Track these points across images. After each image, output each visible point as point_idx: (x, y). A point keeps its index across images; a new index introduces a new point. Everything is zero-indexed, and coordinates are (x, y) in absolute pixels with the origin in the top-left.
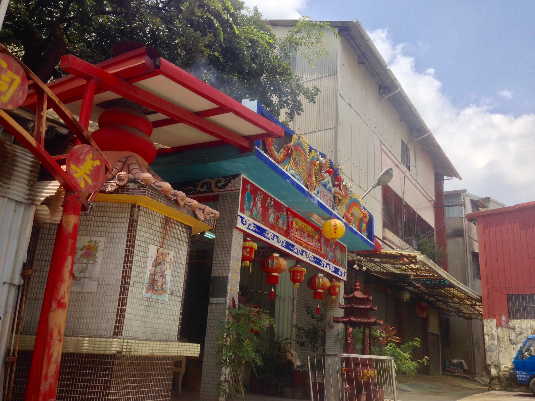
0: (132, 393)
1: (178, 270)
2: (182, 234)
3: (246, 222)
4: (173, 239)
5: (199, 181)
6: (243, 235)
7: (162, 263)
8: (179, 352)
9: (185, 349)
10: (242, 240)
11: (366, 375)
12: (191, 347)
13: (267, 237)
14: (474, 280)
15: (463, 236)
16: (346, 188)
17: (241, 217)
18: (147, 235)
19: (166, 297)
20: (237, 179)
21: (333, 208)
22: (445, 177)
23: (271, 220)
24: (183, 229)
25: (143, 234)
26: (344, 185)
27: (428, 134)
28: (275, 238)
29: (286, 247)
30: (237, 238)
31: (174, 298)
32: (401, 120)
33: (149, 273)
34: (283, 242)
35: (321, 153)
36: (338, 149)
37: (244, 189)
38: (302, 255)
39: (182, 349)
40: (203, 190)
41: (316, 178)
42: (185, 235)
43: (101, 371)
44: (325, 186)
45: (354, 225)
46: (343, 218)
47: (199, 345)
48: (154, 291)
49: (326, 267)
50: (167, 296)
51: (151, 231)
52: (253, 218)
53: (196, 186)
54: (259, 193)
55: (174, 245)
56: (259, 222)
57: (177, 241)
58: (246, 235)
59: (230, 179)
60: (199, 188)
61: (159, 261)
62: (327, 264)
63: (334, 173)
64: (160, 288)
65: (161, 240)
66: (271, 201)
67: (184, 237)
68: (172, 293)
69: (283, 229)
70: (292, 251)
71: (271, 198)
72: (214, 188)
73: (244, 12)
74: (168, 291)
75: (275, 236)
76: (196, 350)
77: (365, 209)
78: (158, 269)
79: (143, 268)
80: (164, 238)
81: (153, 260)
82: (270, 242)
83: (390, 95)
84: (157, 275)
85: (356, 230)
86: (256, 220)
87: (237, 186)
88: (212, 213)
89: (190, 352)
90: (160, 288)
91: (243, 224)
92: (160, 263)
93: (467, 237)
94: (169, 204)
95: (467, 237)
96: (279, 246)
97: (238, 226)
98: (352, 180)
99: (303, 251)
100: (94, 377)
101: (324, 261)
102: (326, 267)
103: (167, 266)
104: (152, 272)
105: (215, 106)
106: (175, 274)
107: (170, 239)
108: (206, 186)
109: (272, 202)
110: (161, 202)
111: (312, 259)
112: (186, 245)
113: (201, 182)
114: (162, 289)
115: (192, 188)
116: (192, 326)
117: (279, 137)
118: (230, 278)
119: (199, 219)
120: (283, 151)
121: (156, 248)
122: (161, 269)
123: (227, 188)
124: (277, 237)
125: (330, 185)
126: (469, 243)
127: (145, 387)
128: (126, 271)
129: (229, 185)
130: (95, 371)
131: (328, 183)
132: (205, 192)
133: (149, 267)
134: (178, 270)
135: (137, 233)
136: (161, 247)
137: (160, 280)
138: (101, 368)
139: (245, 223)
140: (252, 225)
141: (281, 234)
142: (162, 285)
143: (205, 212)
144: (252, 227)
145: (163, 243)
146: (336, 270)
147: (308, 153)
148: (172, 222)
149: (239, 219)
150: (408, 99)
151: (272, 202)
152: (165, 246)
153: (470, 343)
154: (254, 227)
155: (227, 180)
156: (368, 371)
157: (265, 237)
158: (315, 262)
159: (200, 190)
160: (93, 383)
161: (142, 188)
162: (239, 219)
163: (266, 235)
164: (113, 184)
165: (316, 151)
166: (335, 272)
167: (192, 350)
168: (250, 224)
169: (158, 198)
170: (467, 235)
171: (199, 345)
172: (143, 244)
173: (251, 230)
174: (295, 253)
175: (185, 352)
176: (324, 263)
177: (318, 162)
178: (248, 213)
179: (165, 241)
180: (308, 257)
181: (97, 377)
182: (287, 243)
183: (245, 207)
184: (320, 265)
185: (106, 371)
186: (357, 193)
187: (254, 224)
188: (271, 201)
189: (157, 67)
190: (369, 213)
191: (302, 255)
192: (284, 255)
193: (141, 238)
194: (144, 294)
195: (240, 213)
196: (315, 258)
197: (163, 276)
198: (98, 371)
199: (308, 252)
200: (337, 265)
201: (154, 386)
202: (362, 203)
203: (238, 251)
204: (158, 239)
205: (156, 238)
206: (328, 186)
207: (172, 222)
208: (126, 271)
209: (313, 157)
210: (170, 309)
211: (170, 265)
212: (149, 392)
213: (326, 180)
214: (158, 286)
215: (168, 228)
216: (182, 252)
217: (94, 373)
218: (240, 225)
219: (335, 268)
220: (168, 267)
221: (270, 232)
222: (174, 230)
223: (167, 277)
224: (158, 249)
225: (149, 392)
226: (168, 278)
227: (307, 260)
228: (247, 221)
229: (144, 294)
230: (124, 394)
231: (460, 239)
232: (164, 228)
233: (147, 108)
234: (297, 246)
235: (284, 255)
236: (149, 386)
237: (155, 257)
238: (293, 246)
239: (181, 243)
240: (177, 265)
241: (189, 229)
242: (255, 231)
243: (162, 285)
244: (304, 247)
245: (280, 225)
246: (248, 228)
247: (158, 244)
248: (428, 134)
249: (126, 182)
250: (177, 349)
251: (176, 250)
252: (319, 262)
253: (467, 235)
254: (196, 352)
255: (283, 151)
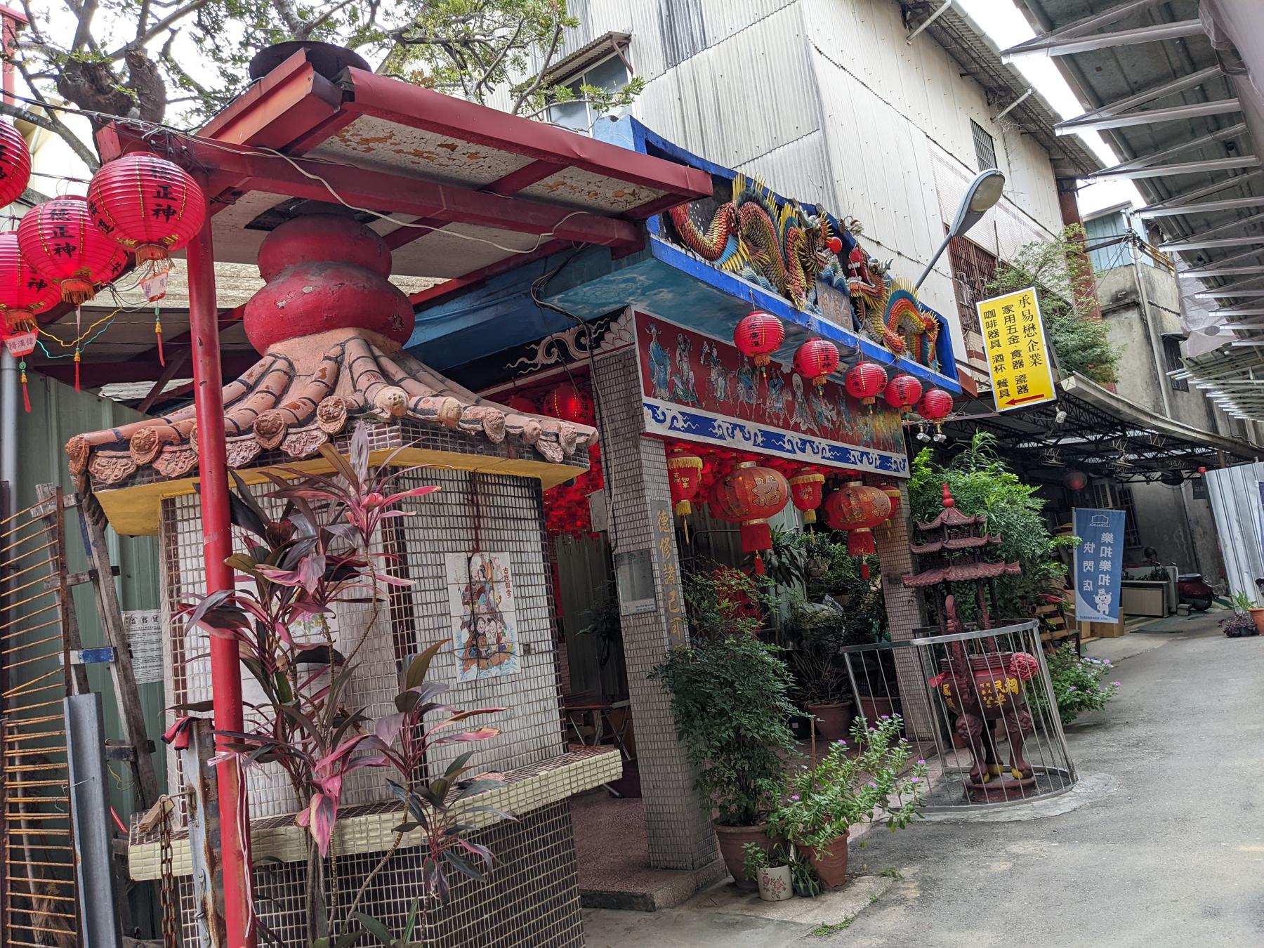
0: (487, 909)
1: (529, 591)
2: (520, 503)
3: (664, 415)
4: (499, 524)
5: (538, 343)
6: (663, 446)
7: (487, 588)
8: (574, 785)
9: (587, 774)
10: (664, 459)
11: (1000, 691)
12: (599, 764)
13: (720, 433)
14: (1175, 395)
15: (1136, 305)
16: (877, 273)
17: (650, 407)
18: (434, 534)
19: (515, 665)
20: (622, 320)
21: (856, 329)
22: (1079, 183)
23: (720, 394)
24: (518, 492)
25: (421, 534)
26: (871, 269)
27: (1030, 91)
28: (737, 432)
29: (766, 444)
30: (651, 457)
31: (534, 659)
32: (961, 75)
33: (460, 623)
34: (756, 435)
35: (805, 206)
36: (836, 178)
37: (644, 339)
38: (803, 450)
39: (581, 776)
40: (552, 360)
41: (805, 268)
42: (527, 503)
43: (400, 882)
44: (829, 281)
45: (908, 353)
46: (882, 344)
47: (618, 751)
48: (483, 662)
49: (861, 461)
50: (518, 661)
51: (441, 522)
52: (679, 401)
53: (533, 354)
54: (680, 339)
55: (506, 535)
56: (693, 406)
57: (511, 524)
58: (670, 445)
59: (608, 323)
60: (541, 359)
61: (478, 587)
62: (863, 454)
63: (845, 245)
64: (494, 648)
65: (471, 534)
66: (711, 349)
67: (523, 506)
68: (527, 650)
69: (750, 405)
70: (781, 448)
71: (710, 341)
72: (573, 351)
73: (1002, 405)
74: (518, 650)
75: (735, 426)
76: (612, 766)
77: (928, 310)
78: (481, 607)
79: (442, 615)
80: (477, 528)
81: (463, 588)
82: (727, 443)
83: (929, 22)
84: (480, 622)
85: (914, 363)
86: (687, 404)
87: (627, 336)
88: (580, 435)
89: (601, 776)
90: (494, 648)
91: (657, 421)
92: (482, 590)
93: (1147, 305)
94: (468, 448)
95: (1147, 305)
96: (748, 446)
97: (649, 429)
98: (878, 243)
99: (804, 442)
100: (388, 898)
101: (855, 450)
102: (861, 461)
103: (501, 590)
104: (467, 619)
105: (528, 160)
106: (524, 603)
107: (491, 524)
108: (555, 350)
109: (715, 351)
110: (444, 449)
111: (828, 454)
112: (535, 525)
113: (543, 342)
114: (502, 649)
115: (526, 361)
116: (592, 701)
117: (701, 197)
118: (654, 551)
119: (553, 462)
120: (718, 227)
121: (464, 556)
122: (488, 603)
123: (605, 346)
124: (742, 428)
125: (840, 275)
126: (1154, 318)
127: (515, 881)
128: (402, 636)
129: (608, 336)
130: (387, 884)
131: (835, 271)
132: (557, 364)
133: (458, 609)
134: (529, 591)
135: (407, 537)
136: (476, 550)
137: (489, 630)
138: (400, 874)
139: (661, 417)
140: (679, 417)
141: (749, 419)
142: (499, 639)
143: (562, 439)
144: (680, 424)
145: (477, 540)
146: (885, 462)
147: (775, 213)
148: (488, 484)
149: (648, 413)
150: (971, 20)
151: (715, 351)
152: (482, 545)
153: (1184, 531)
154: (685, 422)
155: (600, 327)
156: (1004, 683)
157: (714, 436)
158: (836, 459)
159: (545, 362)
160: (389, 912)
161: (387, 429)
162: (648, 413)
163: (716, 431)
164: (315, 433)
165: (791, 202)
166: (882, 466)
167: (605, 765)
168: (674, 418)
169: (435, 441)
170: (1146, 301)
171: (618, 751)
172: (430, 559)
173: (678, 429)
174: (788, 451)
175: (588, 780)
176: (857, 454)
177: (804, 229)
178: (664, 392)
179: (482, 534)
180: (818, 453)
181: (395, 897)
182: (765, 434)
183: (654, 381)
184: (847, 460)
185: (413, 881)
186: (903, 275)
187: (683, 414)
188: (711, 349)
189: (349, 95)
190: (938, 316)
191: (803, 450)
192: (765, 462)
193: (419, 547)
194: (459, 676)
195: (646, 400)
196: (832, 449)
197: (495, 615)
198: (394, 883)
199: (816, 440)
200: (885, 449)
201: (536, 872)
202: (920, 297)
203: (661, 486)
204: (464, 534)
205: (456, 534)
206: (835, 280)
207: (488, 484)
208: (402, 636)
209: (789, 222)
210: (527, 691)
211: (508, 586)
212: (525, 891)
213: (828, 267)
214: (489, 647)
215: (481, 499)
216: (527, 547)
217: (388, 890)
218: (652, 427)
219: (881, 457)
220: (503, 594)
221: (722, 420)
222: (499, 501)
223: (506, 617)
224: (469, 559)
225: (525, 891)
226: (510, 618)
227: (817, 459)
228: (667, 412)
229: (459, 676)
230: (467, 918)
231: (1133, 315)
232: (473, 504)
233: (76, 438)
234: (789, 434)
235: (765, 462)
236: (523, 877)
237: (464, 579)
238: (780, 437)
239: (522, 525)
240: (524, 580)
241: (533, 484)
242: (687, 430)
243: (499, 639)
244: (803, 432)
245: (743, 398)
246: (672, 428)
247: (464, 545)
248: (1030, 91)
249: (342, 421)
250: (567, 781)
251: (513, 546)
252: (843, 455)
253: (1146, 301)
254: (614, 772)
255: (718, 227)
